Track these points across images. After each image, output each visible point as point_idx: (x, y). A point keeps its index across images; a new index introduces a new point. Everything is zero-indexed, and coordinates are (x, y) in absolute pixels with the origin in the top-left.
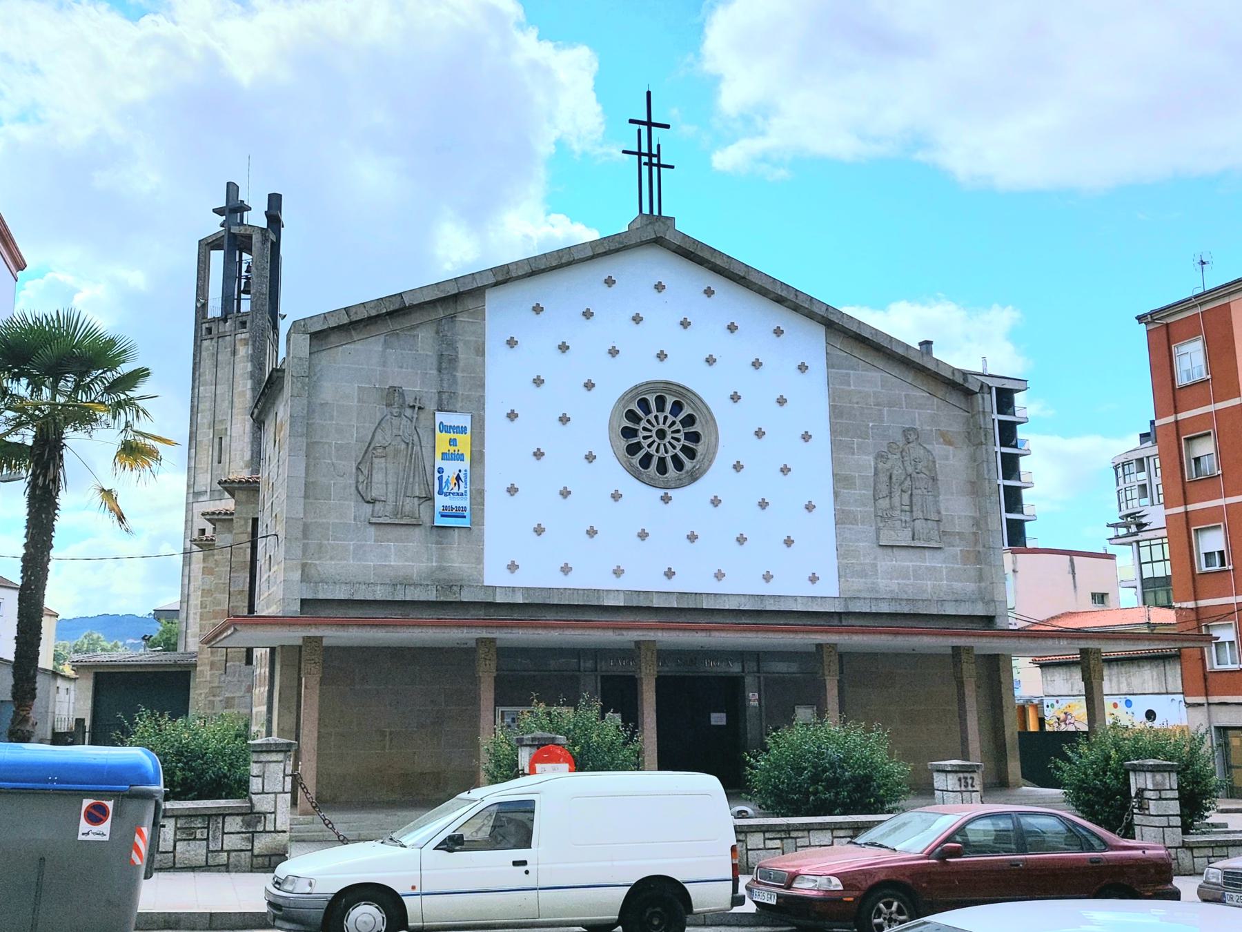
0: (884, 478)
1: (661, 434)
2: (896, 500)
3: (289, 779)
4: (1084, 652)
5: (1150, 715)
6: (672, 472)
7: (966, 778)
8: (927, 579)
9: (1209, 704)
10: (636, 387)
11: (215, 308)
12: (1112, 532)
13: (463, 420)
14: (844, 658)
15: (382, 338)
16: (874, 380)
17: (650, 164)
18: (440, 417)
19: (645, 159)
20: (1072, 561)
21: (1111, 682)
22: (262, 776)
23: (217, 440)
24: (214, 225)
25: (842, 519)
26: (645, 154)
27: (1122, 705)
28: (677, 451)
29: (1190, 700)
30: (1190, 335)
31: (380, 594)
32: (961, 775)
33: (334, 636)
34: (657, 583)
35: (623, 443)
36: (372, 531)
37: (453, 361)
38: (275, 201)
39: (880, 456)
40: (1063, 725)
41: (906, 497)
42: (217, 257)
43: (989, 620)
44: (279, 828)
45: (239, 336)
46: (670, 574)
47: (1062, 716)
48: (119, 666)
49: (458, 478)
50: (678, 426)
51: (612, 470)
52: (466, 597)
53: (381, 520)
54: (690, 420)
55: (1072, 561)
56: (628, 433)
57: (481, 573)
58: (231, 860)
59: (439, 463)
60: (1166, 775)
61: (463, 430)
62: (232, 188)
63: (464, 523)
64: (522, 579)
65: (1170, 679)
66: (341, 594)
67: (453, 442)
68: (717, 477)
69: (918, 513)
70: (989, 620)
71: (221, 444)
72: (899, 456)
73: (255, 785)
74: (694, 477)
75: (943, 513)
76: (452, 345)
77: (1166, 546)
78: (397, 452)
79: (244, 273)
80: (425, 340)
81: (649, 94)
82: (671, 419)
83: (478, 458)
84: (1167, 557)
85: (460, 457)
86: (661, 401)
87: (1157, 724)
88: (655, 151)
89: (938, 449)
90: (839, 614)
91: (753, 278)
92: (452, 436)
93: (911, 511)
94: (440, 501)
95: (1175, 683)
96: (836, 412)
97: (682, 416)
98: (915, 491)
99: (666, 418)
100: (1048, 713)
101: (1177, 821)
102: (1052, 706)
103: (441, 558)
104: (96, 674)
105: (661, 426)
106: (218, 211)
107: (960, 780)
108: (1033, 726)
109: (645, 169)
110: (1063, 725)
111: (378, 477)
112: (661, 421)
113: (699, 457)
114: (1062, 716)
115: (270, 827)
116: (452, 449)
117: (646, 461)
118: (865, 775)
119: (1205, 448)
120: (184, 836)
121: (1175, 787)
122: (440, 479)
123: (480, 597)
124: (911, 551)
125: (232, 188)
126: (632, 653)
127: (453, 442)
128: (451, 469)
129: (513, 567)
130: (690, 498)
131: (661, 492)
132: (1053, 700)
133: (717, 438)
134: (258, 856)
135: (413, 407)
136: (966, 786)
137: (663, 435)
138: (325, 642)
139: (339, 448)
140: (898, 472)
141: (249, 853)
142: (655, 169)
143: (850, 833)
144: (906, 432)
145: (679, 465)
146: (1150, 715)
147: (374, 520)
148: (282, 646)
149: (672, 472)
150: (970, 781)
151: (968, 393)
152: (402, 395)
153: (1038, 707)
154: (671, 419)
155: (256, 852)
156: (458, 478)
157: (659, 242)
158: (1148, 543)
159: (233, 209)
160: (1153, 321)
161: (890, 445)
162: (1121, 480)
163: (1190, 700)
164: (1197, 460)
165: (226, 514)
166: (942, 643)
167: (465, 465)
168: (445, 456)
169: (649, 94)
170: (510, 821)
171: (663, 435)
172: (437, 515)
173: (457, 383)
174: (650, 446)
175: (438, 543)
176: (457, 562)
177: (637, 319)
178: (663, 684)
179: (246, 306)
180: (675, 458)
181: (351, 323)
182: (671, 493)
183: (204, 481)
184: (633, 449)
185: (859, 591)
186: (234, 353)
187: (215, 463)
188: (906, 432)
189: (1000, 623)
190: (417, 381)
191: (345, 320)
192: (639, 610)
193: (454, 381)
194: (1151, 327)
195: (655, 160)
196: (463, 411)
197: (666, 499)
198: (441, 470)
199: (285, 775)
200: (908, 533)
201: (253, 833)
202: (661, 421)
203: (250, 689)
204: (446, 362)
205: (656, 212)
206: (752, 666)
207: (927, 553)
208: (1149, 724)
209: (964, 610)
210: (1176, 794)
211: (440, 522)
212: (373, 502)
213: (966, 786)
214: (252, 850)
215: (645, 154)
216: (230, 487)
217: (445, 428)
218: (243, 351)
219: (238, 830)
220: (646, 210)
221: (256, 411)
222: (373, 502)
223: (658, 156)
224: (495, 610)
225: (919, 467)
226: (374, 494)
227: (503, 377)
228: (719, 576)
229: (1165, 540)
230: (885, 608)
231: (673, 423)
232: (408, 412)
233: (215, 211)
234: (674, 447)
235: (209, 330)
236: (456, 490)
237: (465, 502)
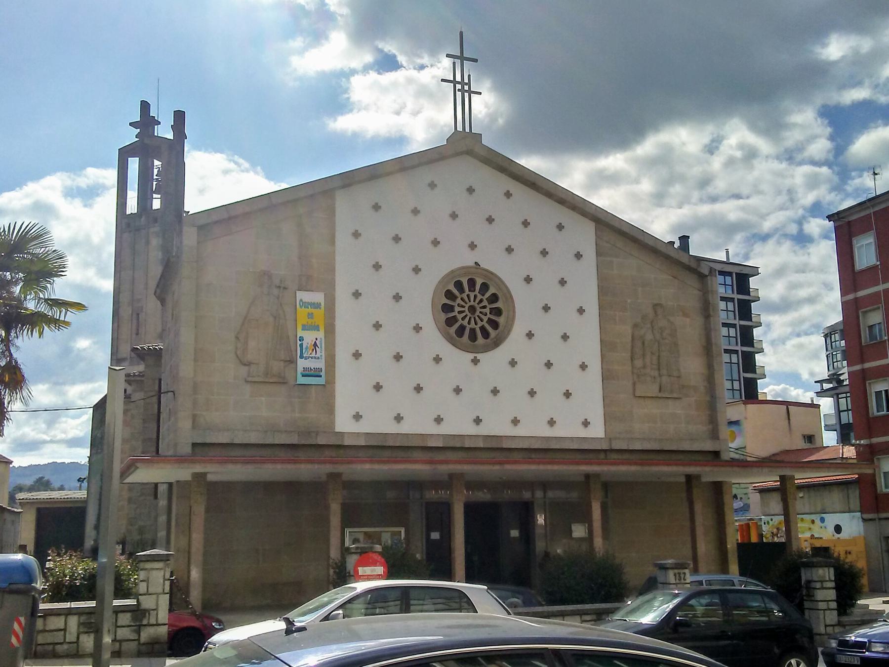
0: (639, 344)
1: (472, 309)
2: (648, 360)
3: (168, 583)
4: (783, 479)
5: (838, 529)
6: (480, 340)
7: (679, 574)
8: (669, 422)
9: (880, 519)
10: (452, 271)
11: (132, 206)
12: (818, 387)
13: (318, 297)
14: (607, 486)
16: (632, 265)
17: (462, 91)
18: (302, 296)
19: (459, 87)
20: (788, 409)
21: (801, 503)
22: (146, 580)
23: (135, 316)
24: (131, 136)
25: (607, 376)
26: (459, 83)
27: (818, 522)
28: (485, 323)
29: (866, 516)
30: (864, 231)
31: (253, 438)
32: (676, 571)
33: (217, 472)
35: (443, 317)
36: (248, 388)
38: (179, 117)
39: (635, 326)
40: (776, 539)
41: (655, 358)
42: (134, 164)
43: (716, 454)
44: (160, 622)
45: (152, 230)
46: (478, 421)
47: (775, 531)
48: (56, 502)
49: (315, 345)
50: (485, 303)
51: (434, 339)
52: (321, 441)
53: (256, 379)
54: (494, 298)
55: (788, 409)
56: (446, 308)
57: (333, 423)
58: (123, 648)
59: (300, 333)
60: (826, 569)
61: (317, 306)
62: (145, 106)
63: (321, 381)
64: (364, 427)
65: (851, 501)
66: (223, 439)
67: (310, 316)
68: (514, 343)
69: (664, 372)
70: (716, 454)
71: (138, 319)
72: (649, 326)
73: (142, 588)
74: (497, 344)
77: (849, 399)
79: (155, 177)
82: (479, 297)
83: (330, 330)
84: (850, 408)
85: (317, 328)
86: (472, 283)
87: (844, 535)
88: (466, 81)
89: (679, 320)
90: (605, 451)
92: (310, 310)
94: (302, 364)
95: (855, 502)
96: (603, 291)
97: (488, 295)
99: (475, 296)
100: (765, 528)
101: (834, 605)
102: (768, 523)
104: (39, 510)
105: (472, 303)
107: (675, 575)
108: (754, 539)
109: (459, 94)
110: (776, 539)
111: (252, 344)
112: (472, 298)
113: (501, 328)
114: (775, 531)
115: (153, 621)
116: (310, 321)
117: (461, 331)
119: (876, 318)
120: (86, 630)
121: (833, 579)
122: (301, 345)
123: (333, 441)
125: (145, 106)
126: (450, 482)
127: (310, 316)
128: (309, 337)
129: (357, 417)
130: (493, 361)
131: (471, 356)
132: (769, 518)
133: (514, 312)
134: (144, 644)
135: (279, 287)
136: (680, 580)
137: (474, 312)
140: (649, 337)
141: (136, 642)
142: (466, 95)
143: (594, 617)
144: (655, 306)
145: (486, 335)
146: (838, 529)
147: (250, 379)
148: (178, 481)
149: (480, 340)
150: (682, 576)
151: (702, 277)
152: (270, 277)
153: (759, 527)
154: (479, 297)
155: (143, 640)
156: (315, 345)
157: (469, 153)
158: (844, 395)
159: (146, 121)
160: (839, 219)
161: (644, 317)
162: (829, 348)
163: (866, 516)
164: (871, 327)
165: (139, 376)
166: (675, 472)
167: (320, 335)
168: (305, 328)
170: (24, 504)
171: (474, 312)
172: (299, 375)
174: (463, 319)
177: (526, 224)
178: (471, 509)
179: (156, 204)
180: (483, 329)
181: (230, 218)
183: (125, 350)
184: (450, 322)
185: (620, 433)
186: (148, 243)
187: (134, 336)
188: (655, 306)
189: (725, 456)
191: (226, 216)
192: (456, 448)
194: (838, 223)
195: (466, 88)
196: (317, 290)
198: (301, 339)
199: (165, 580)
200: (656, 387)
201: (140, 626)
202: (472, 298)
203: (156, 518)
205: (467, 130)
206: (539, 494)
207: (670, 402)
208: (838, 536)
209: (696, 447)
210: (832, 584)
211: (301, 380)
212: (248, 364)
213: (680, 580)
214: (138, 640)
215: (459, 83)
216: (140, 355)
217: (305, 305)
218: (155, 242)
219: (128, 624)
220: (460, 128)
221: (158, 291)
222: (248, 364)
223: (469, 84)
224: (341, 449)
225: (664, 334)
226: (250, 357)
228: (515, 422)
229: (848, 395)
230: (638, 446)
231: (481, 301)
232: (275, 291)
233: (131, 124)
235: (128, 225)
236: (313, 355)
237: (321, 364)
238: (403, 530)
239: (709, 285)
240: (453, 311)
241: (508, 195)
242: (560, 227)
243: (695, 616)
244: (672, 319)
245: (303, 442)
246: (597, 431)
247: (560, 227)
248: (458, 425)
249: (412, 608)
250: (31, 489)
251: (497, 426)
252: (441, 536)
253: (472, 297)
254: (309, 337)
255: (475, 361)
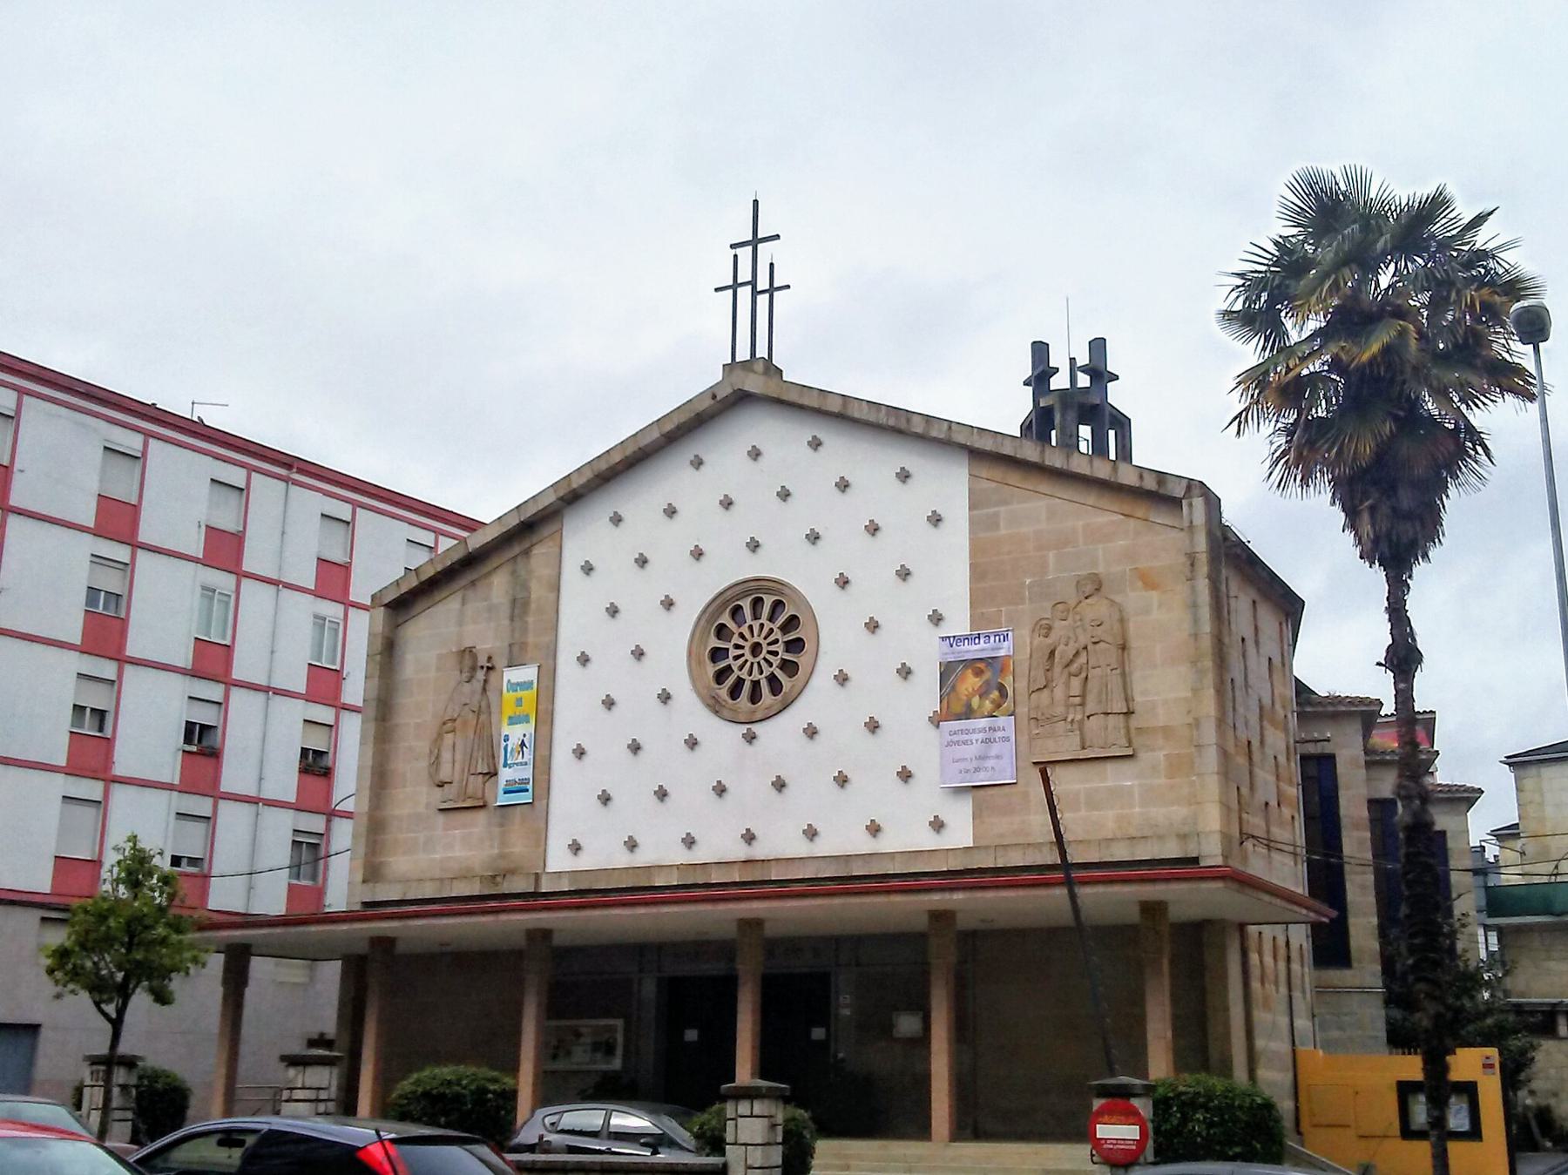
15: (459, 595)
31: (428, 892)
34: (862, 844)
35: (803, 660)
36: (441, 818)
37: (526, 603)
41: (1076, 684)
54: (793, 622)
75: (1138, 698)
76: (526, 587)
78: (465, 723)
80: (498, 585)
81: (756, 202)
91: (645, 441)
93: (1082, 704)
94: (506, 775)
98: (1092, 673)
103: (503, 843)
106: (1026, 383)
118: (478, 1088)
124: (1084, 767)
126: (725, 949)
131: (744, 729)
138: (401, 948)
139: (418, 726)
151: (1174, 503)
167: (529, 728)
169: (756, 202)
171: (754, 650)
173: (532, 629)
175: (502, 825)
176: (519, 847)
182: (755, 728)
190: (487, 638)
193: (525, 631)
197: (750, 738)
200: (1075, 739)
204: (519, 606)
207: (1110, 767)
211: (503, 800)
227: (578, 616)
234: (771, 665)
238: (619, 1023)
239: (370, 754)
240: (787, 643)
241: (816, 444)
242: (904, 476)
243: (137, 1087)
244: (1118, 599)
245: (486, 892)
246: (960, 833)
247: (904, 476)
248: (719, 845)
249: (236, 1108)
250: (1529, 928)
251: (782, 842)
252: (808, 1034)
253: (758, 628)
254: (516, 733)
255: (750, 738)
